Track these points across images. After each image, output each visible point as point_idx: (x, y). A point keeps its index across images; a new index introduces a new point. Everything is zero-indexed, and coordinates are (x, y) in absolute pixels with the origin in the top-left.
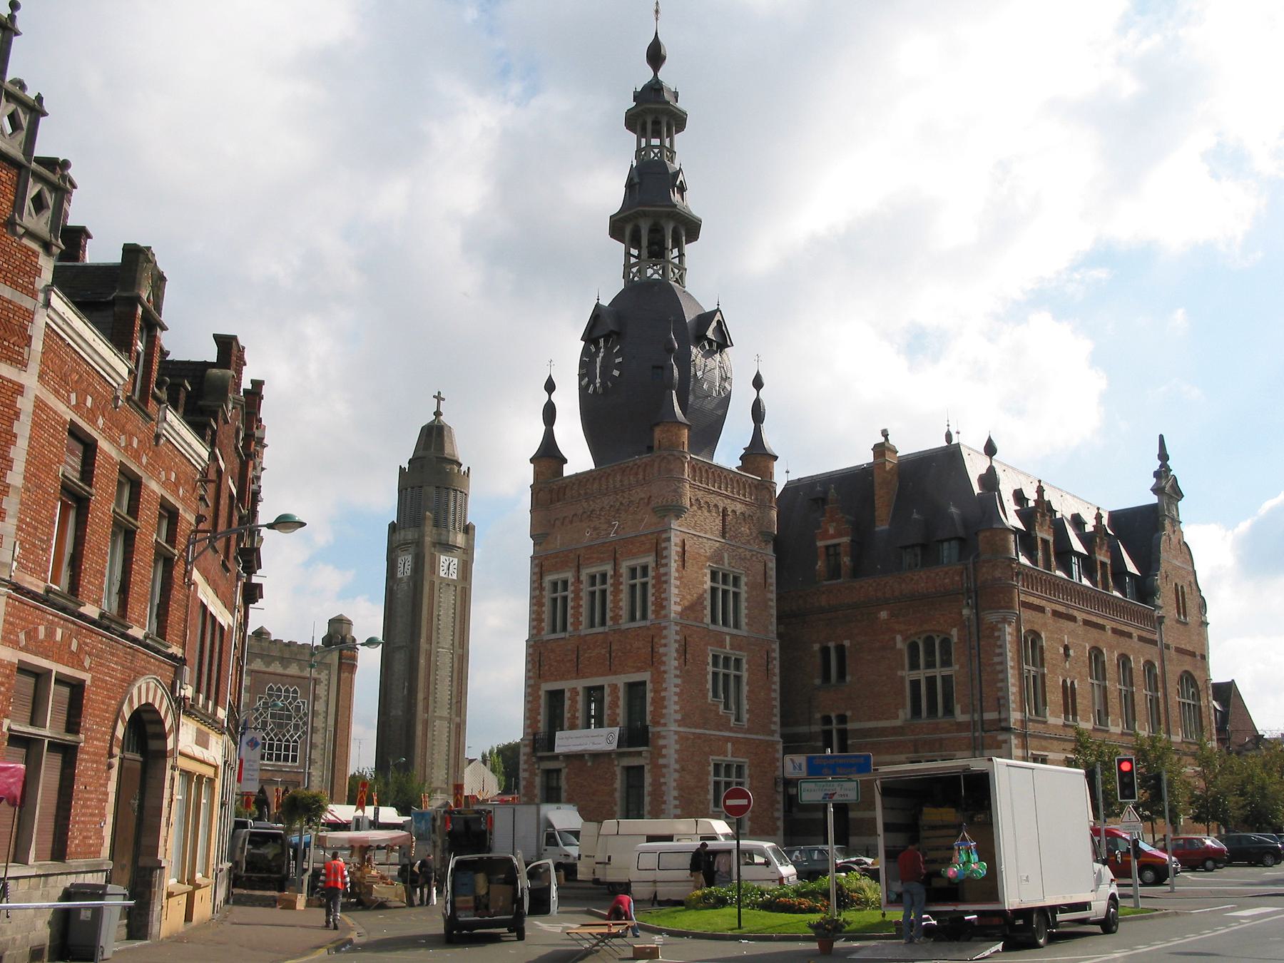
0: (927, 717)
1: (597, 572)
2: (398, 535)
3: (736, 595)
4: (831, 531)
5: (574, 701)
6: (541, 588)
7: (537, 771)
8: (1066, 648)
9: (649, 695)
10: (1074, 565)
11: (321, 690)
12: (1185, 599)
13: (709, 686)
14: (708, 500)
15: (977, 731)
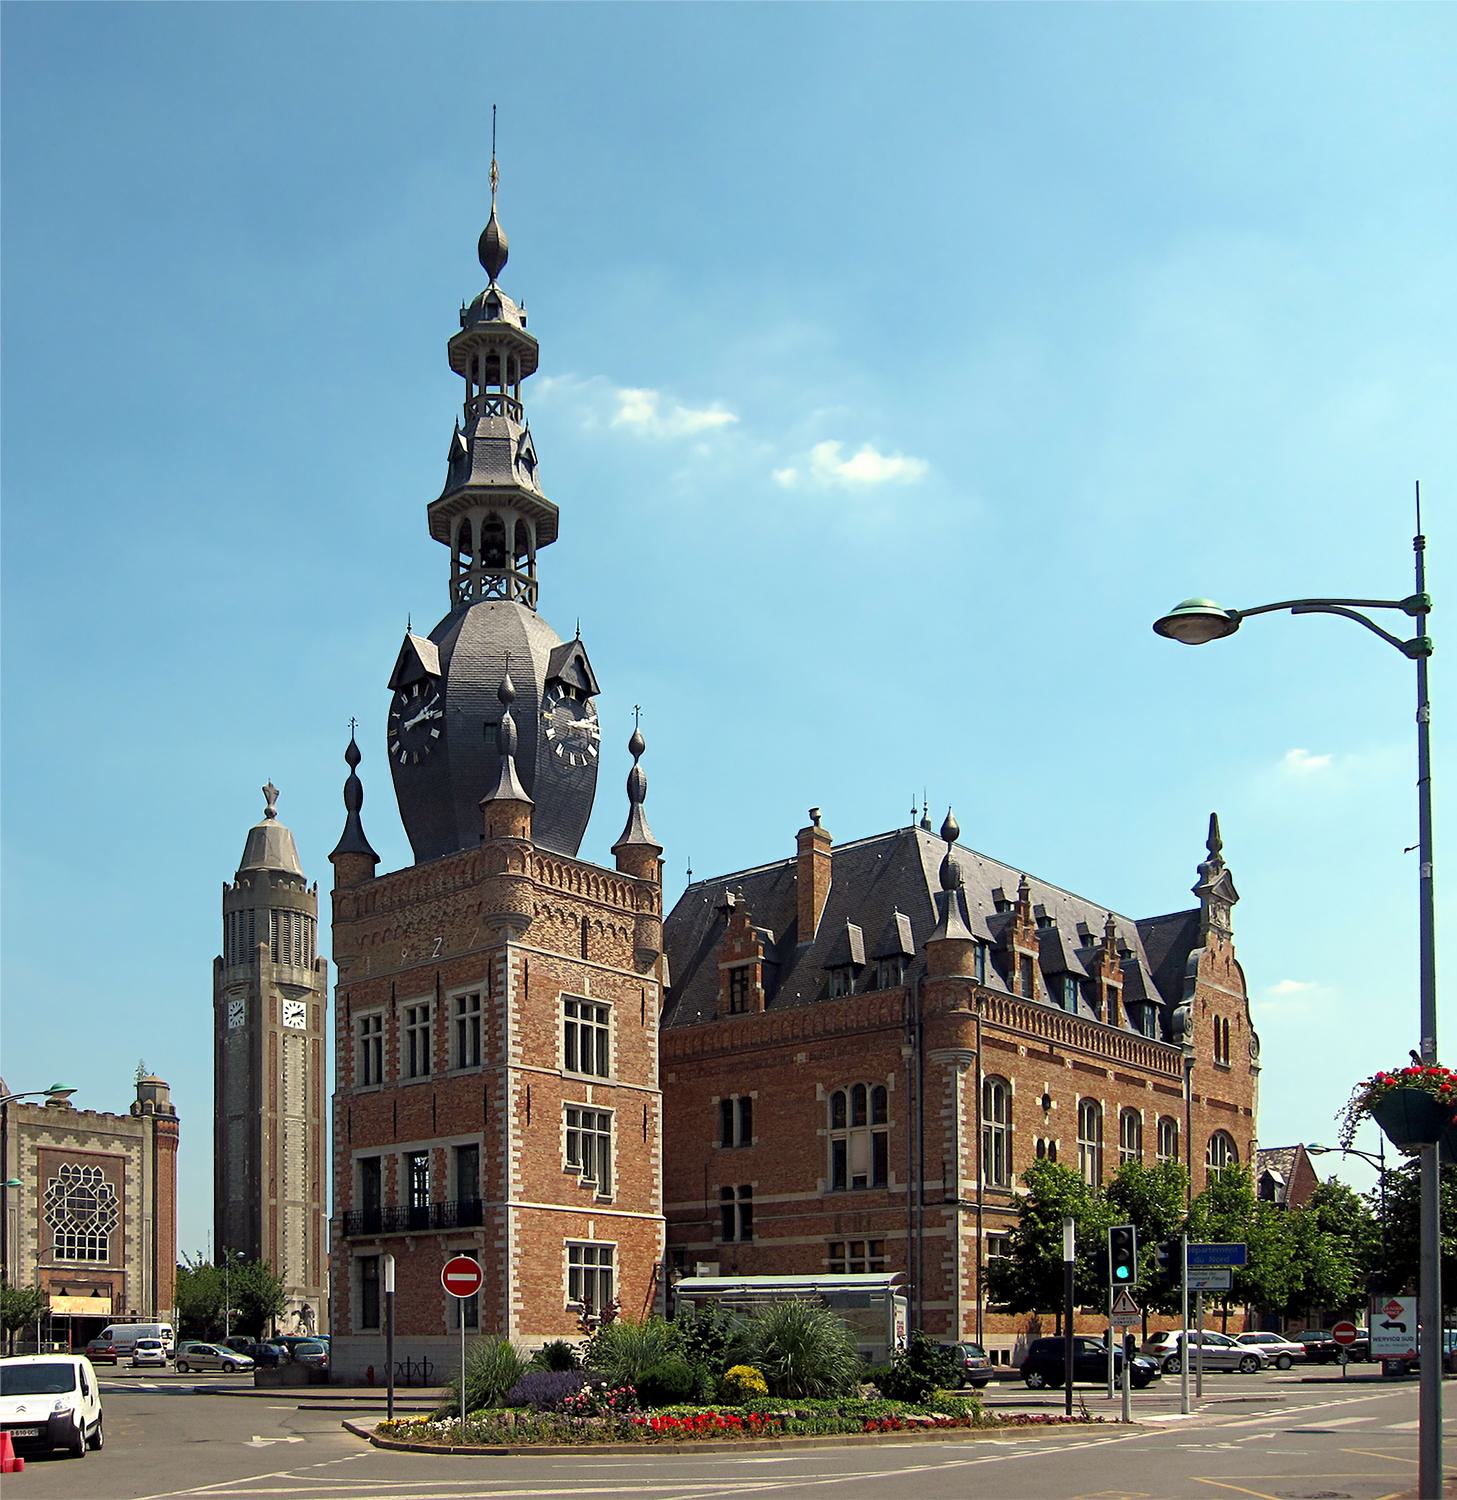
0: (854, 1188)
1: (417, 1005)
2: (226, 973)
3: (602, 1033)
4: (738, 949)
5: (392, 1171)
6: (349, 1028)
7: (350, 1259)
8: (1046, 1099)
9: (483, 1162)
10: (1066, 992)
11: (131, 1170)
12: (1228, 1037)
13: (563, 1149)
14: (561, 907)
15: (915, 1205)
